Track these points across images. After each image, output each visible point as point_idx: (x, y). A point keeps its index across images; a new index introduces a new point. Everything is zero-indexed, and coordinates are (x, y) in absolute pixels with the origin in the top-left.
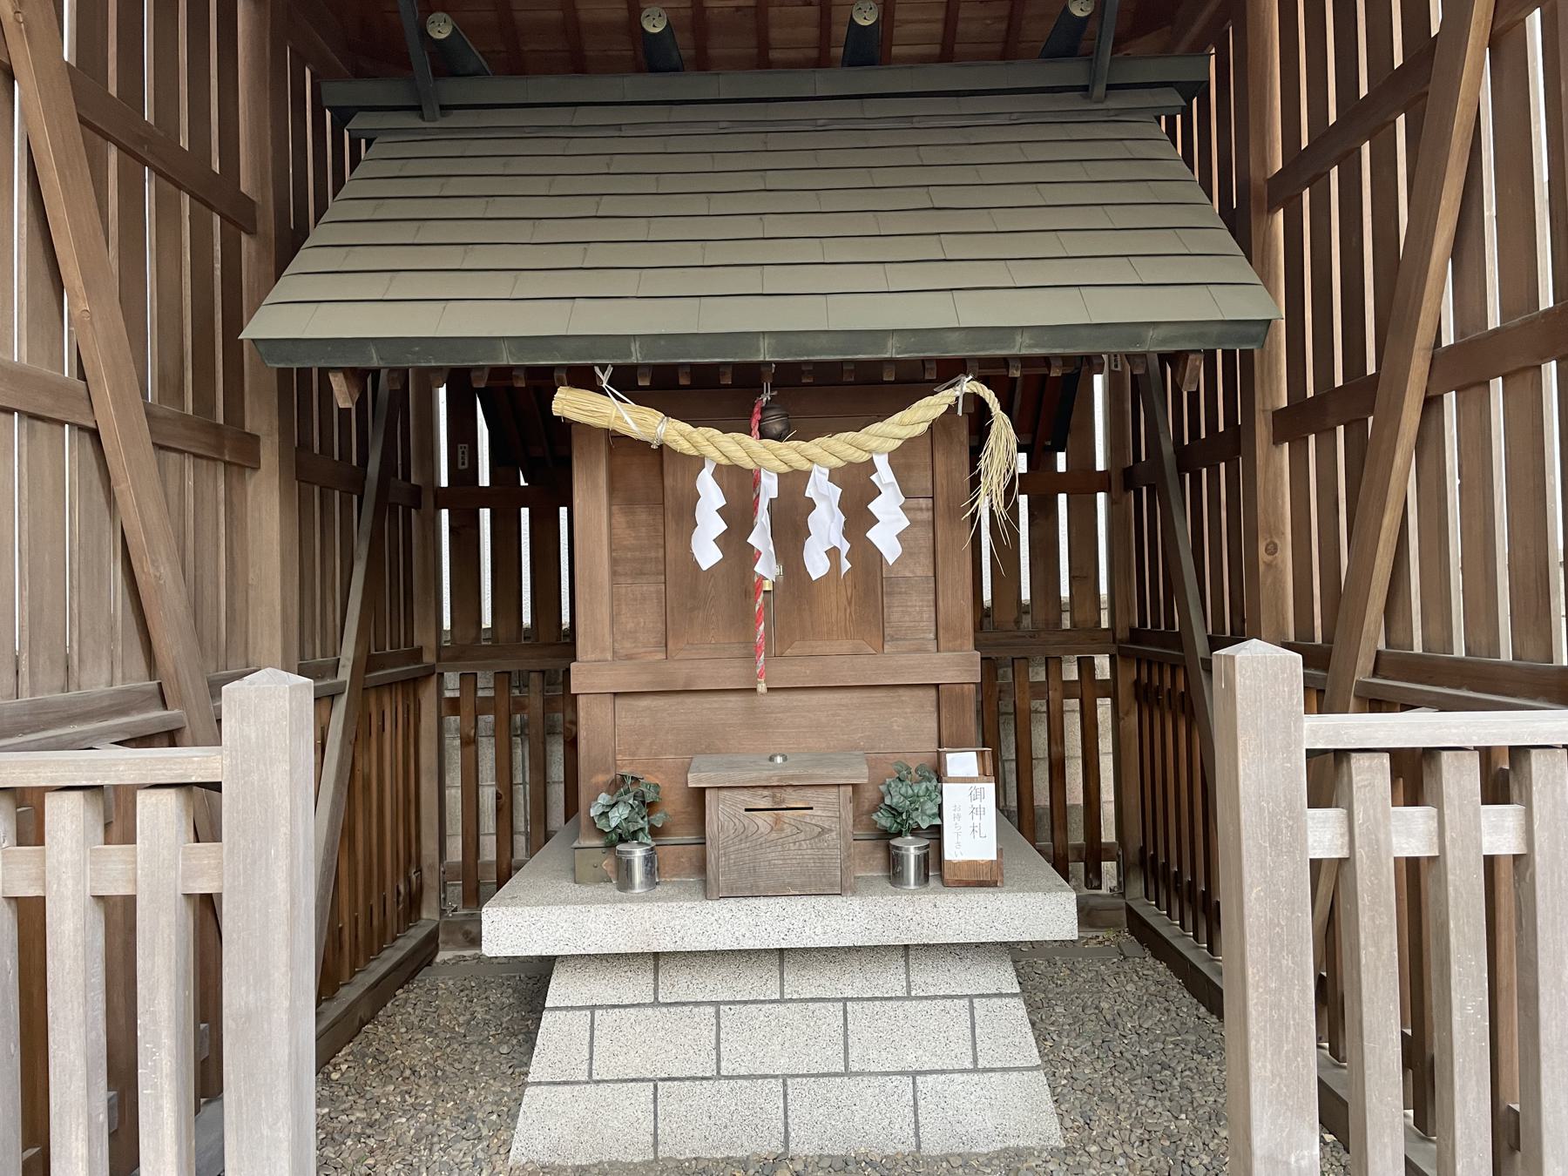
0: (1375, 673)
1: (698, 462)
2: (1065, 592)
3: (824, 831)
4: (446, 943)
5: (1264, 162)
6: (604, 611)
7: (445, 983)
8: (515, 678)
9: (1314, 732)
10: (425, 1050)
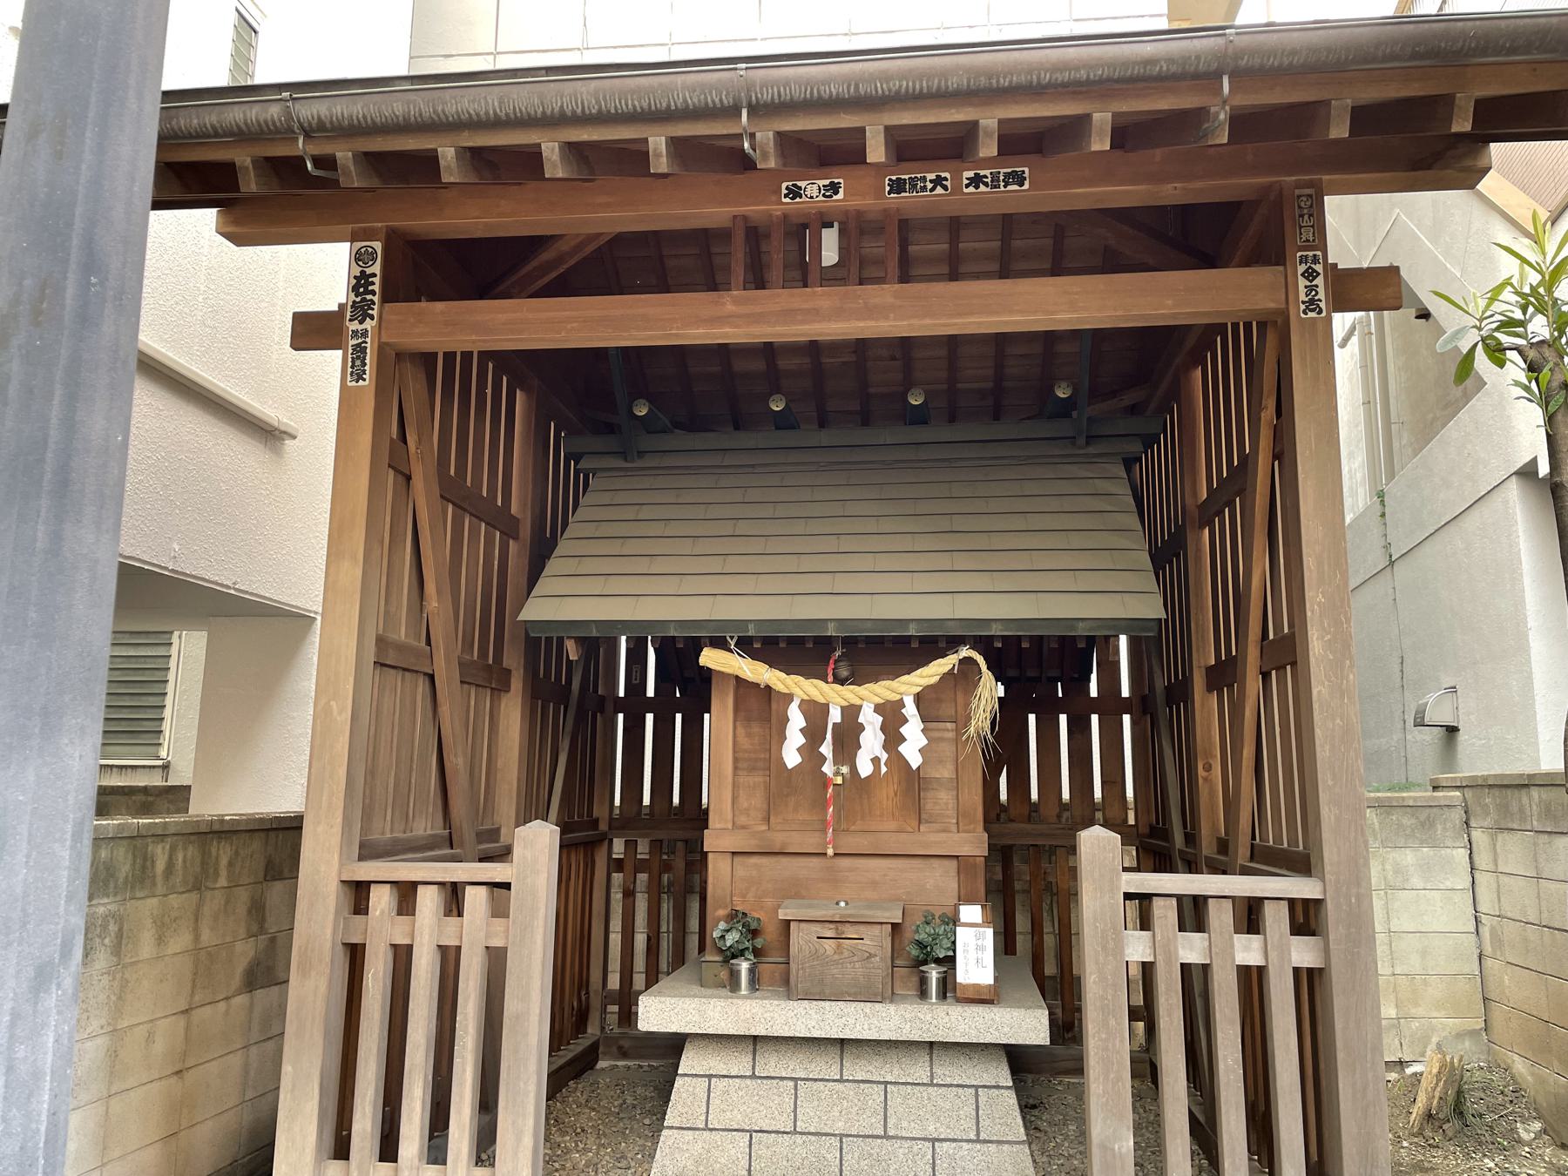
0: (1252, 858)
1: (789, 698)
2: (1098, 794)
3: (871, 956)
4: (604, 1054)
5: (1195, 494)
6: (727, 794)
7: (603, 1081)
8: (665, 845)
9: (1128, 882)
10: (590, 1119)
